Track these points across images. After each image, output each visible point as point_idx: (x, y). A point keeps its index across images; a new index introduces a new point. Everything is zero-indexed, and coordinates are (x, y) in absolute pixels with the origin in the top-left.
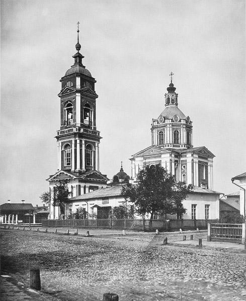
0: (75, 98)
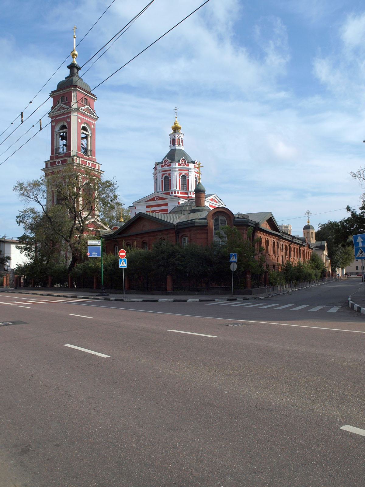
0: (70, 117)
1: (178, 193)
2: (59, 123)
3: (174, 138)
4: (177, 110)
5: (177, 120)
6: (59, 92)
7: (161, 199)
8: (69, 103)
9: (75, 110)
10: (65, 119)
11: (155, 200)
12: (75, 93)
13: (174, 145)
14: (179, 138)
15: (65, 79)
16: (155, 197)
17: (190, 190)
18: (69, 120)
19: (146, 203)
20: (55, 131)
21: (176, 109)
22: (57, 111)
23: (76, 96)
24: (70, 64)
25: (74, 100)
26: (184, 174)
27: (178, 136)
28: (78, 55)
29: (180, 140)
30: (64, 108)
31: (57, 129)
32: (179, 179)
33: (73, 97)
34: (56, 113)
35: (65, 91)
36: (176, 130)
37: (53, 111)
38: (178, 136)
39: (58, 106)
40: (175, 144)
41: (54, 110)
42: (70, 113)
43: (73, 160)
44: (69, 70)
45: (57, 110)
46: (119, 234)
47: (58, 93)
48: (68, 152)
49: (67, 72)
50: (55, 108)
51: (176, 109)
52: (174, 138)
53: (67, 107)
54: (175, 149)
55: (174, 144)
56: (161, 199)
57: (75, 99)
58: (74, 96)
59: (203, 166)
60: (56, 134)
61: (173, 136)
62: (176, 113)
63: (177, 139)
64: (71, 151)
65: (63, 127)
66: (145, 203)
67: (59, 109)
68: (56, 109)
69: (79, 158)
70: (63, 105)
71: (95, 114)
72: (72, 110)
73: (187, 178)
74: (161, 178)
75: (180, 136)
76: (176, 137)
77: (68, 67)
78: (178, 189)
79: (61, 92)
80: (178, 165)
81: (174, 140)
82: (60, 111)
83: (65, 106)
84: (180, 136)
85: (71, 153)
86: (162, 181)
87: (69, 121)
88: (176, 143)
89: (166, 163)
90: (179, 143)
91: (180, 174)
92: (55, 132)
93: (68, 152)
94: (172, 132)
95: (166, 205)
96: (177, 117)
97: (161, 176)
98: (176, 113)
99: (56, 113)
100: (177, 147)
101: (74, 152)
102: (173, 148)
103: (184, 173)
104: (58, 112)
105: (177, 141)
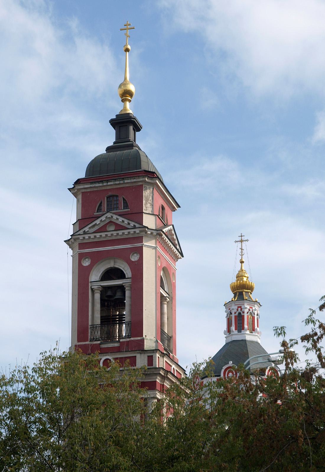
0: (140, 251)
2: (103, 262)
3: (240, 313)
4: (244, 243)
5: (243, 268)
6: (105, 184)
8: (137, 215)
9: (152, 233)
10: (124, 255)
12: (148, 191)
13: (240, 331)
14: (252, 314)
15: (105, 152)
18: (134, 258)
20: (90, 281)
21: (242, 241)
22: (94, 232)
23: (151, 198)
24: (117, 116)
25: (147, 208)
27: (251, 309)
28: (134, 93)
29: (253, 318)
30: (119, 227)
31: (95, 276)
33: (144, 202)
34: (89, 237)
35: (124, 183)
36: (244, 293)
38: (239, 309)
39: (103, 218)
40: (243, 328)
41: (90, 228)
42: (140, 239)
43: (151, 360)
44: (112, 132)
45: (96, 228)
47: (101, 185)
48: (132, 339)
49: (109, 137)
50: (93, 223)
51: (242, 241)
52: (240, 313)
53: (132, 224)
54: (245, 341)
55: (240, 327)
57: (149, 205)
58: (147, 200)
59: (187, 366)
60: (92, 290)
61: (236, 307)
62: (242, 249)
63: (248, 316)
64: (142, 336)
65: (113, 273)
67: (105, 226)
68: (96, 224)
69: (163, 357)
70: (121, 219)
71: (178, 247)
72: (144, 233)
75: (254, 308)
76: (246, 311)
77: (114, 123)
79: (109, 184)
81: (240, 318)
82: (103, 234)
83: (126, 221)
84: (255, 310)
85: (143, 341)
87: (133, 260)
88: (246, 326)
92: (90, 284)
93: (132, 339)
94: (230, 296)
96: (243, 260)
98: (242, 249)
99: (92, 236)
100: (249, 337)
101: (151, 340)
102: (236, 336)
104: (98, 235)
105: (248, 322)
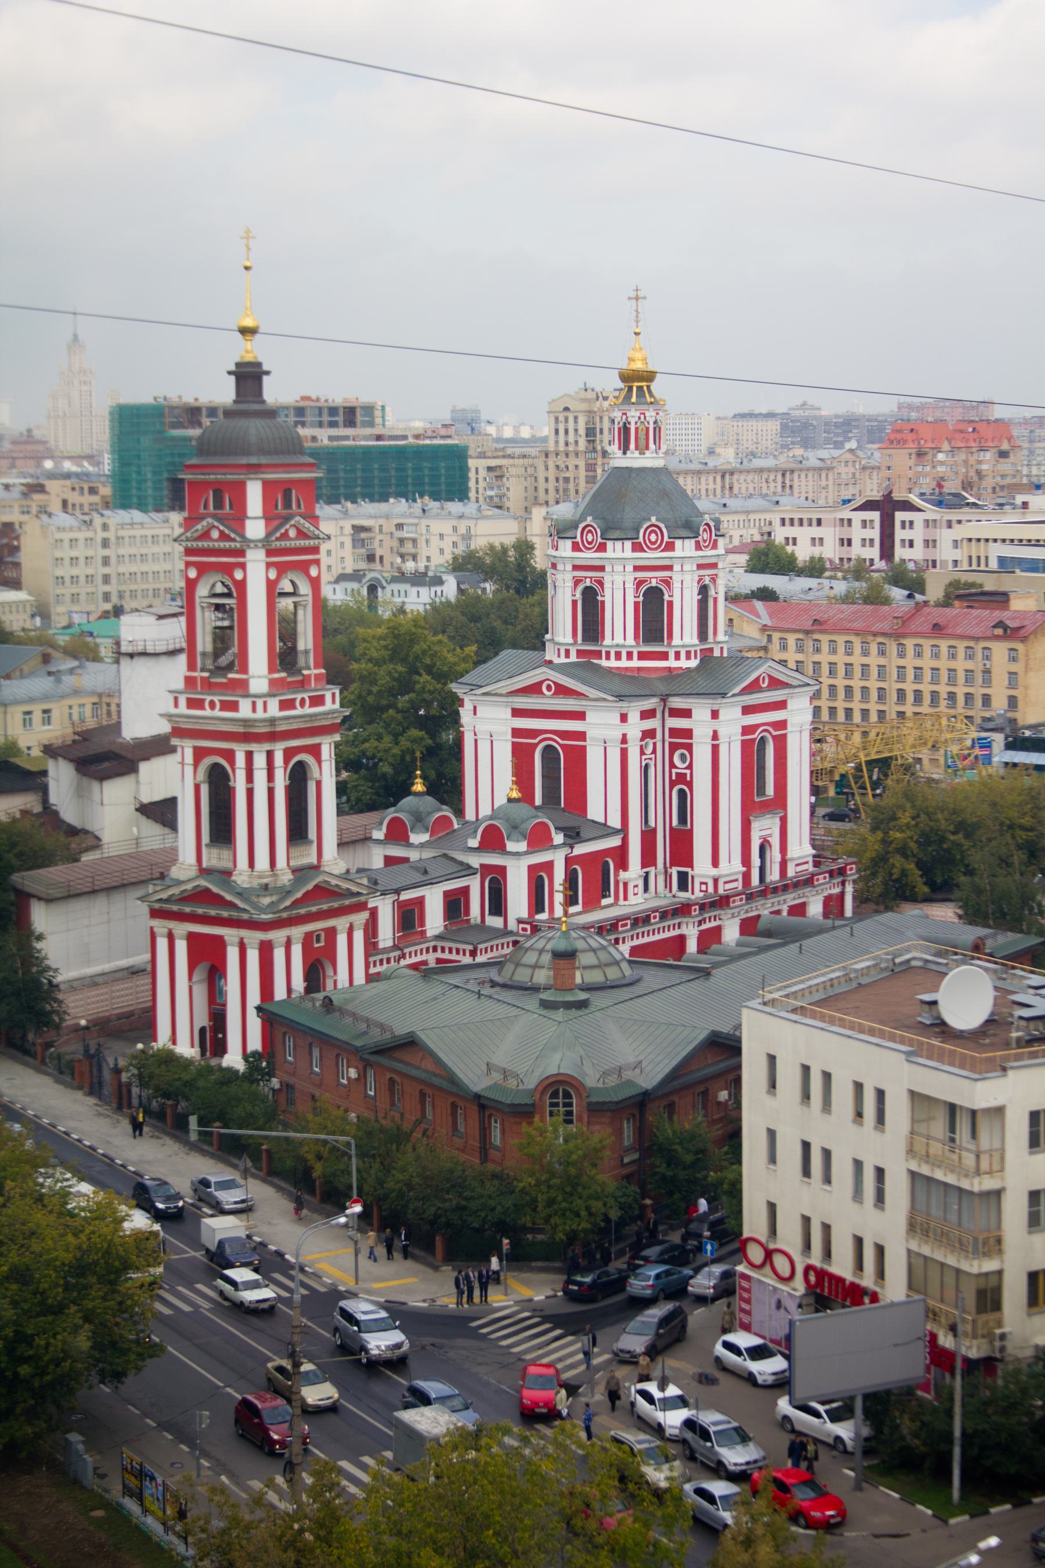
1: (630, 656)
4: (640, 301)
7: (562, 691)
11: (542, 693)
16: (543, 682)
17: (676, 641)
18: (238, 575)
19: (510, 699)
26: (654, 581)
29: (647, 429)
32: (636, 604)
37: (189, 534)
46: (377, 1052)
51: (637, 298)
56: (562, 691)
63: (637, 429)
66: (505, 699)
73: (666, 597)
74: (568, 591)
78: (630, 640)
80: (634, 550)
86: (574, 603)
89: (590, 537)
90: (642, 442)
91: (639, 583)
95: (580, 716)
97: (570, 584)
103: (654, 579)
